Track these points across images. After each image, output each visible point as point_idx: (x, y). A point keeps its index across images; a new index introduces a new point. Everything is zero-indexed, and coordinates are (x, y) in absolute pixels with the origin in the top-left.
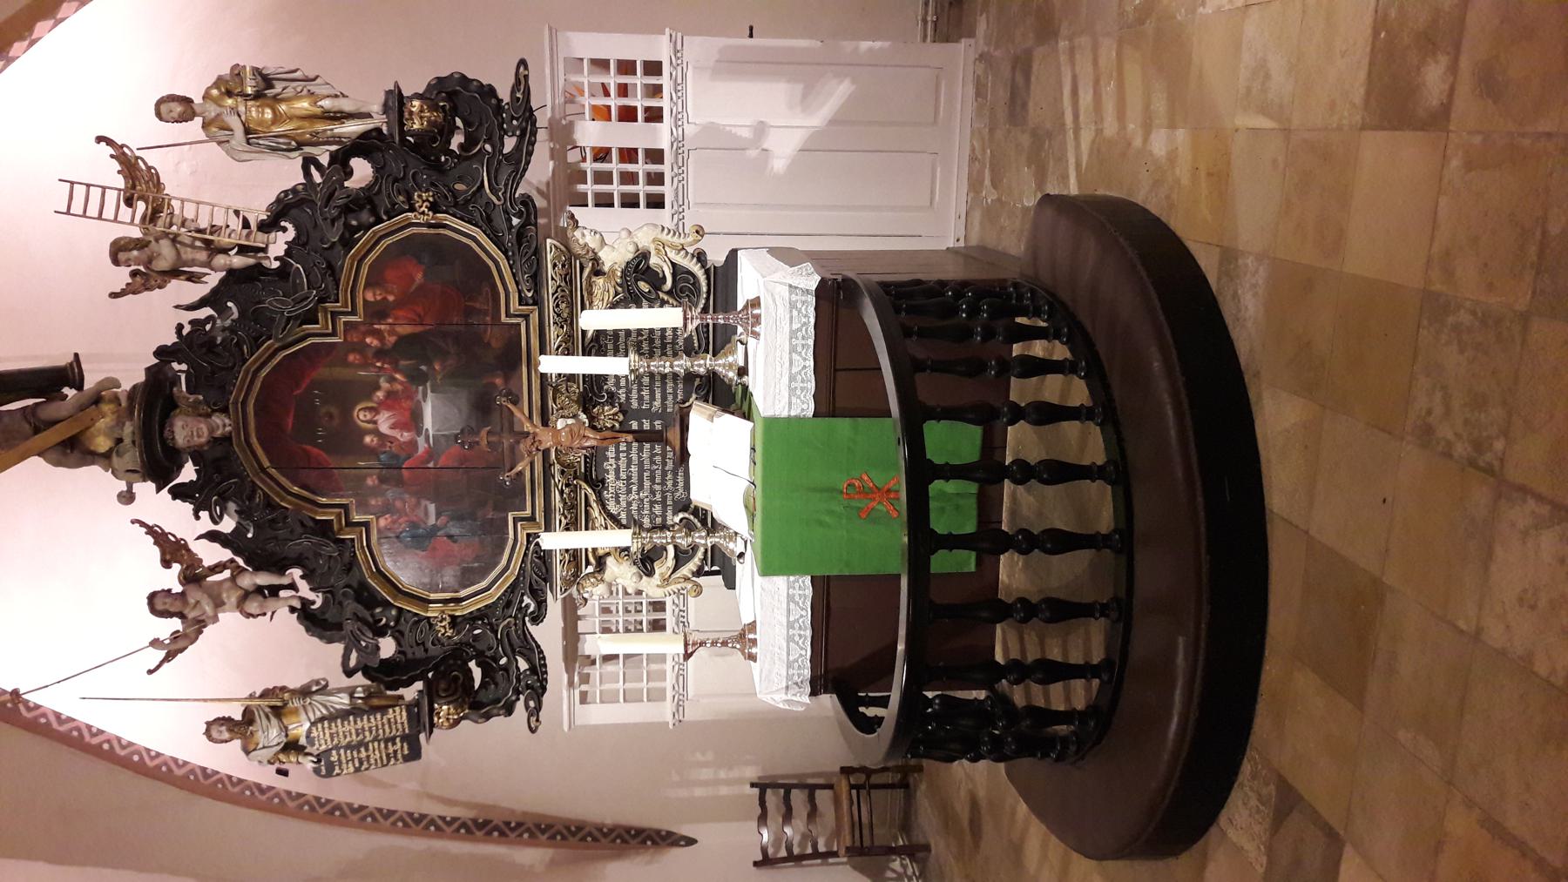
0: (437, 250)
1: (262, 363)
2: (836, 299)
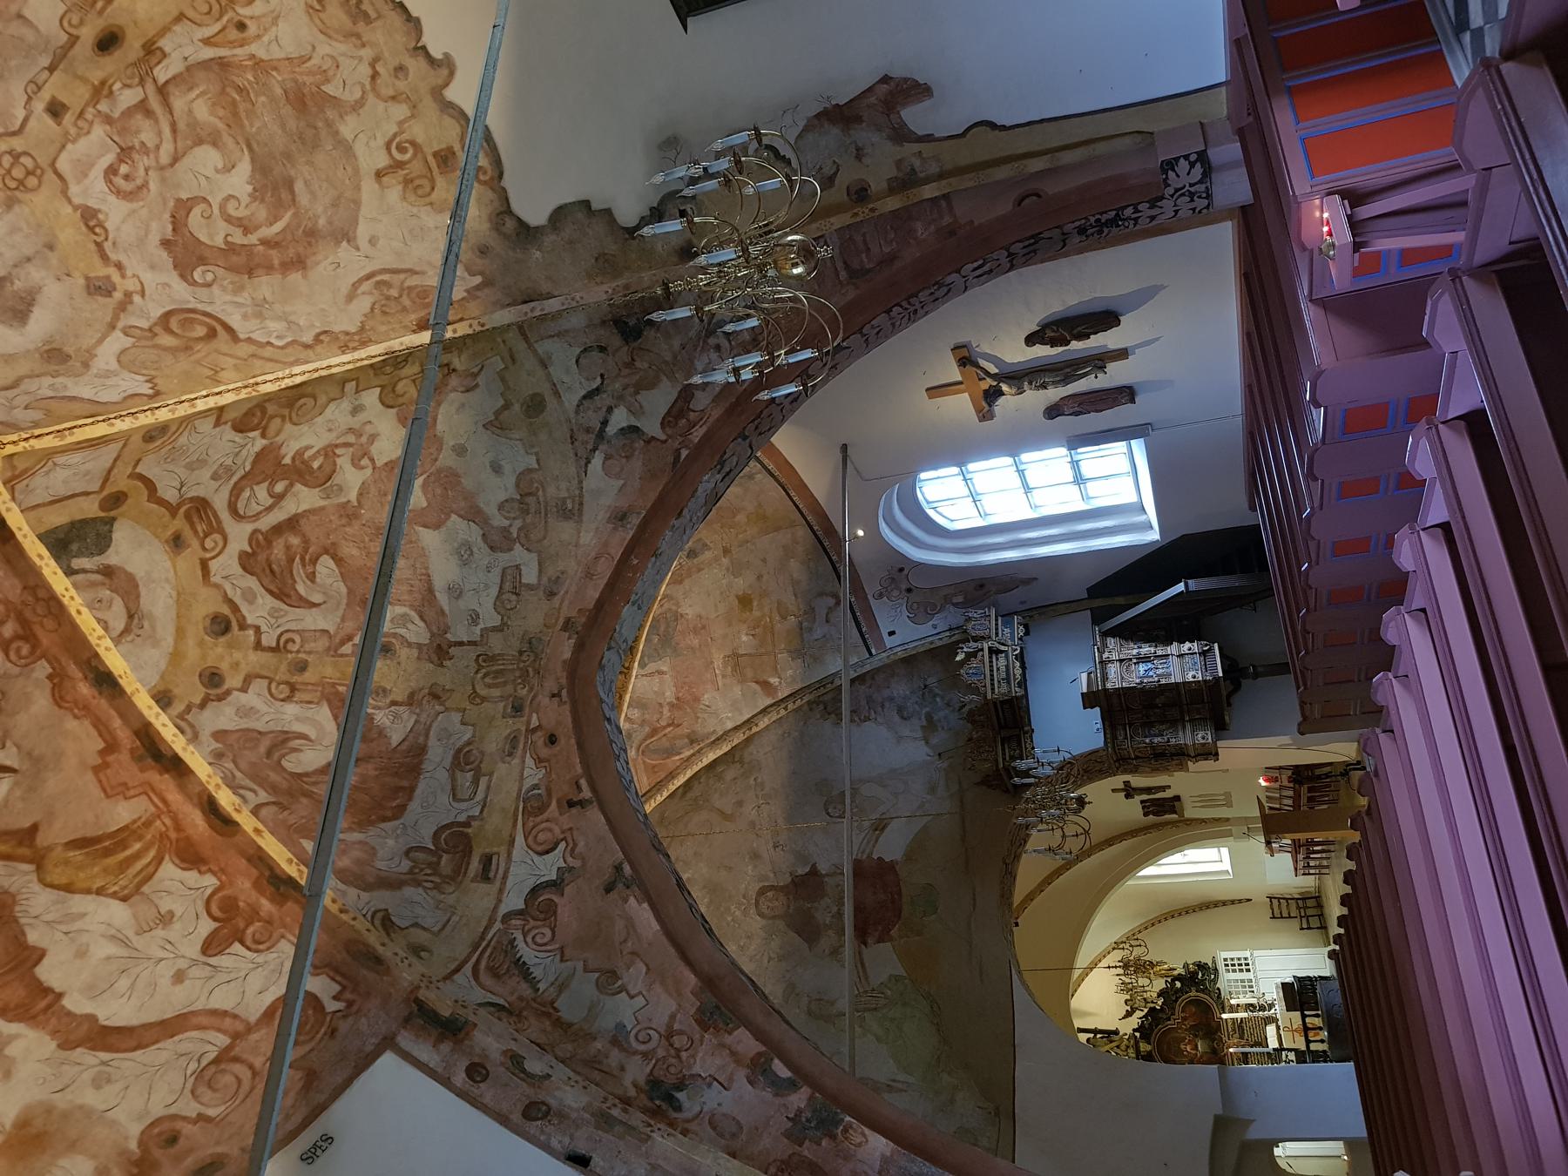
0: (1197, 1002)
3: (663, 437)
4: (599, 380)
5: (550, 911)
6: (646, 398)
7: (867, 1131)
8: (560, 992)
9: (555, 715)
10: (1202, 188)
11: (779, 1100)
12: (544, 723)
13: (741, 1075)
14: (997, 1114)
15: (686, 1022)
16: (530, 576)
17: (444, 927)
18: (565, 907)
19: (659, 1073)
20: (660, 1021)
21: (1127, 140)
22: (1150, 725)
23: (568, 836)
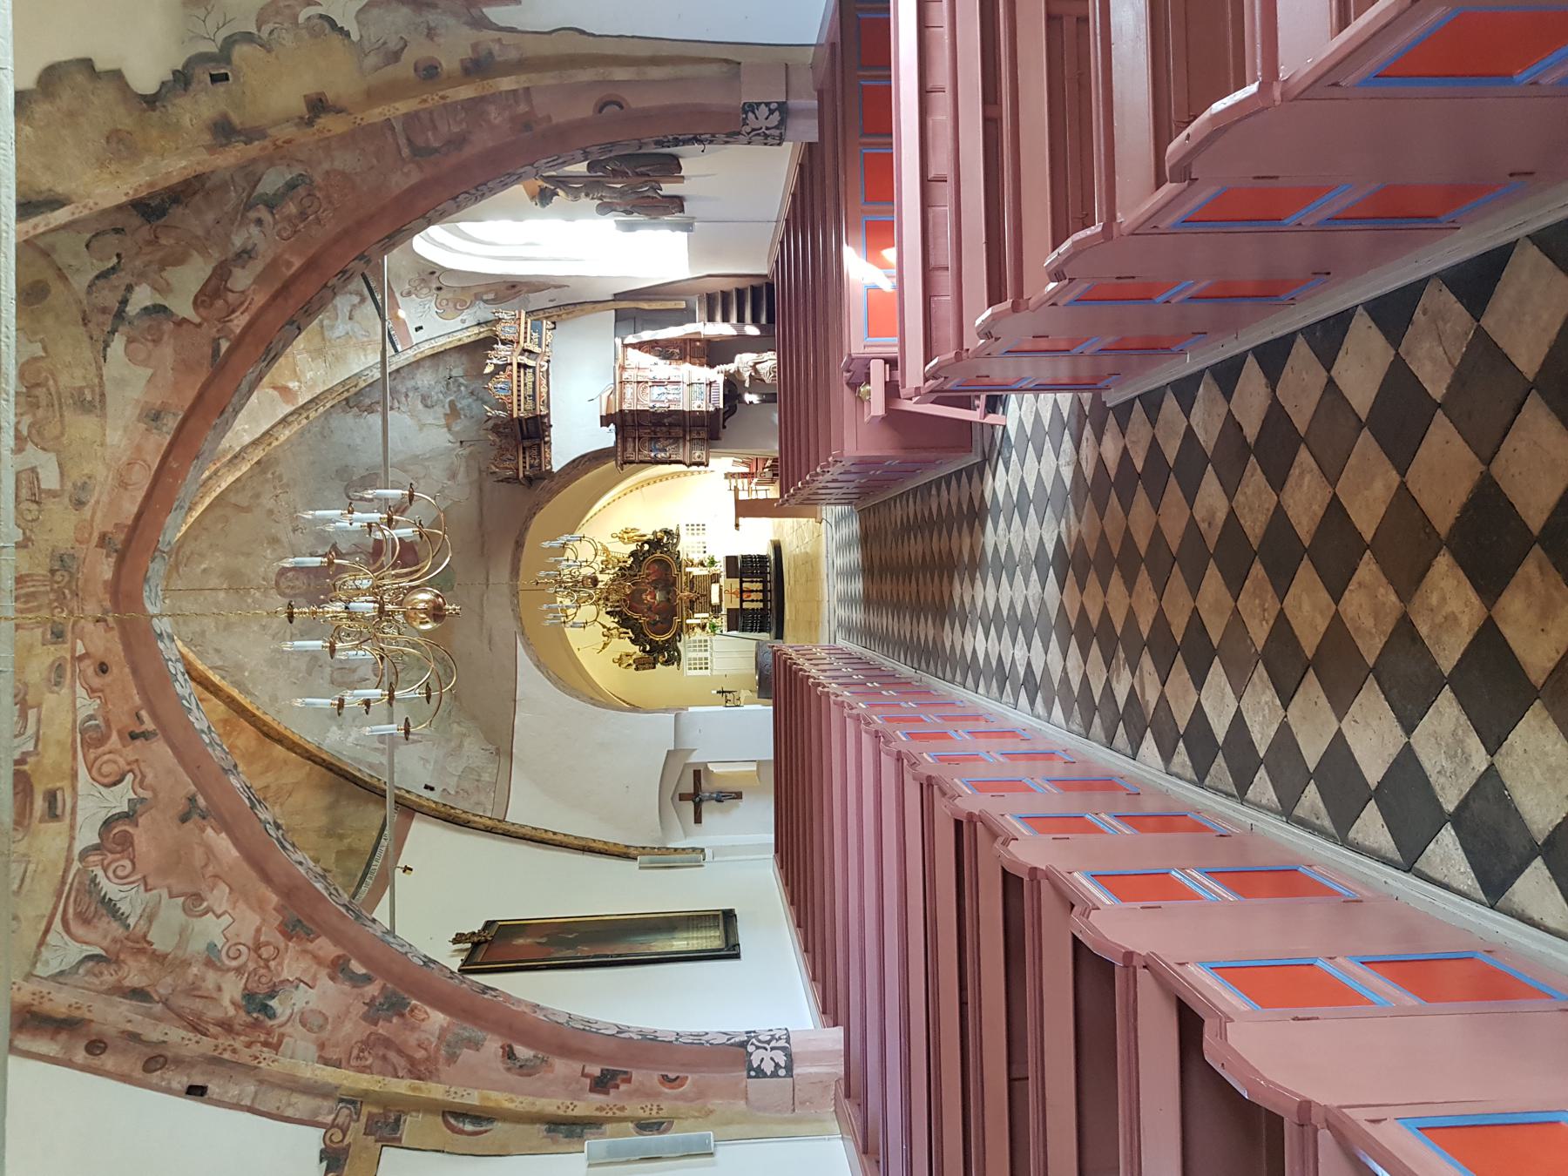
0: (660, 561)
3: (197, 320)
4: (115, 260)
5: (126, 842)
6: (172, 274)
7: (428, 1009)
8: (150, 922)
9: (101, 640)
10: (777, 132)
11: (356, 991)
12: (92, 650)
13: (323, 974)
14: (498, 754)
15: (271, 935)
16: (50, 479)
17: (22, 880)
20: (247, 936)
21: (715, 67)
22: (657, 440)
23: (133, 767)
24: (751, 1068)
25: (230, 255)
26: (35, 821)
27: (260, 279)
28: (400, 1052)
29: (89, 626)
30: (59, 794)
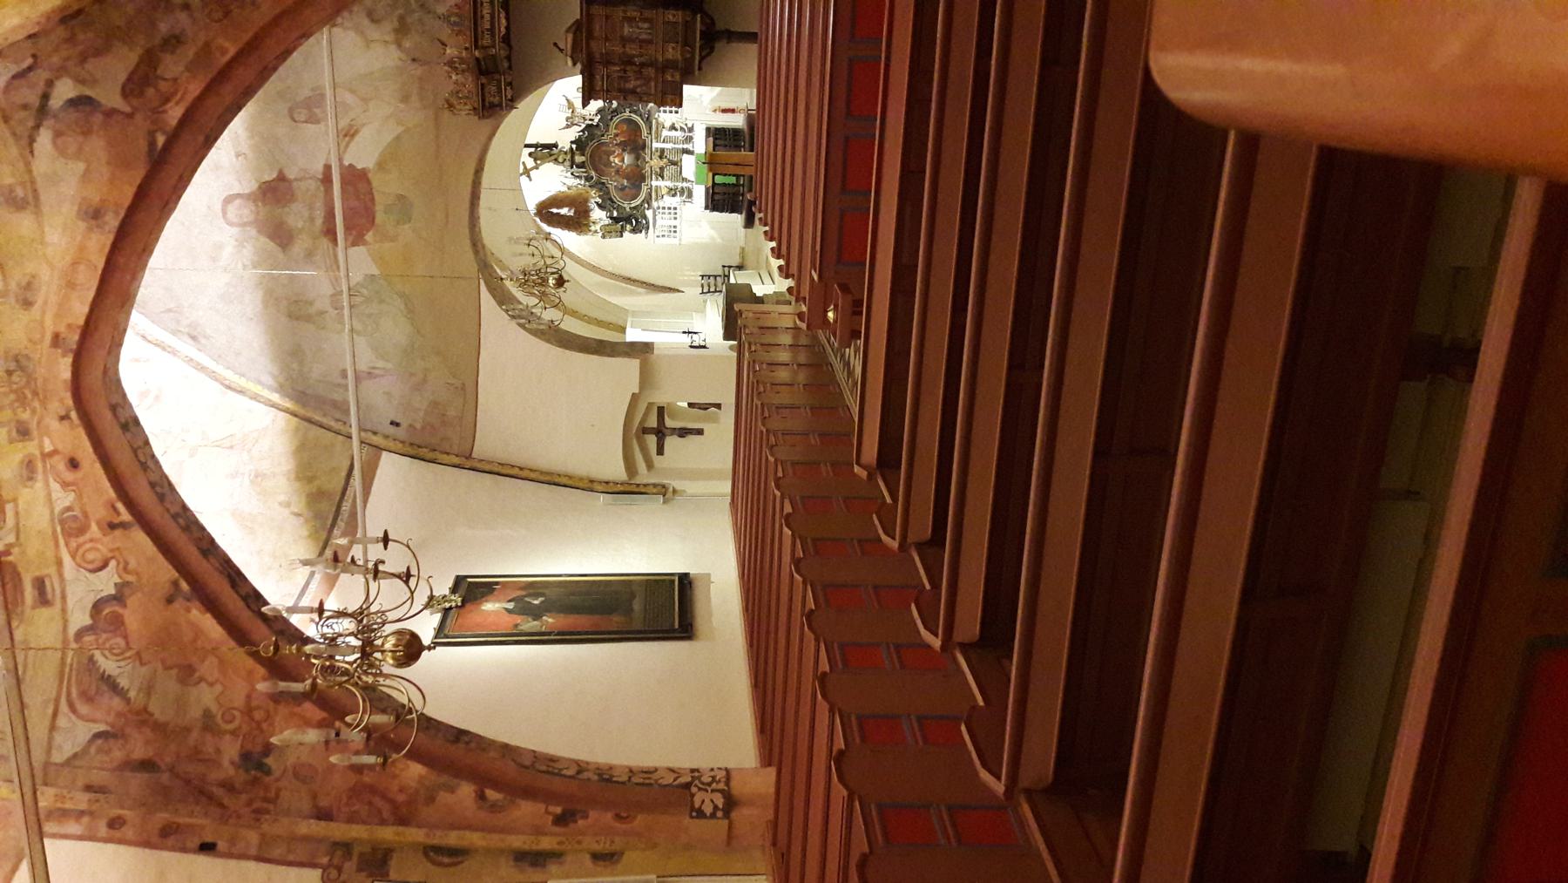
0: (630, 121)
1: (593, 144)
2: (708, 129)
3: (128, 109)
5: (117, 623)
12: (60, 447)
18: (132, 617)
19: (249, 747)
20: (239, 701)
23: (116, 553)
24: (692, 808)
25: (157, 41)
26: (28, 611)
27: (192, 67)
28: (384, 797)
29: (54, 424)
30: (47, 583)
